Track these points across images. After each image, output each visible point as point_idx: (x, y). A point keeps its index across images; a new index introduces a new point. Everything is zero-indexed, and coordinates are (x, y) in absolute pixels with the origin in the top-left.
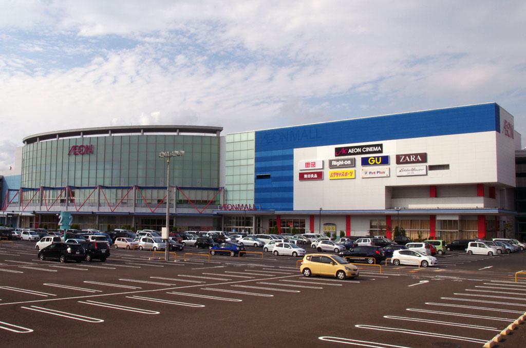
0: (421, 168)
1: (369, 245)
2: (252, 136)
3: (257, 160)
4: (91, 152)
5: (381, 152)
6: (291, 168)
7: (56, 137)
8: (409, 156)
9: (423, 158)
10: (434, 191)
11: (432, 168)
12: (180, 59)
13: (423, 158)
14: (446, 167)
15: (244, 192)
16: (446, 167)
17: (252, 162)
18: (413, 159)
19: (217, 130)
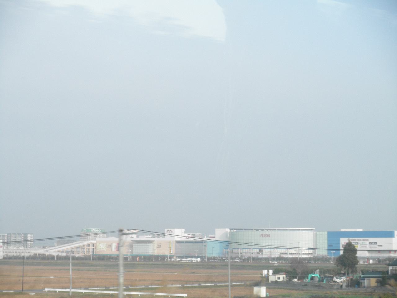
0: (375, 246)
1: (165, 229)
2: (326, 233)
3: (328, 240)
4: (269, 236)
5: (214, 237)
6: (339, 243)
7: (72, 292)
8: (373, 242)
9: (376, 243)
10: (379, 251)
11: (378, 246)
12: (313, 287)
13: (378, 244)
14: (381, 246)
15: (321, 247)
16: (381, 246)
17: (326, 241)
18: (374, 243)
19: (160, 245)
